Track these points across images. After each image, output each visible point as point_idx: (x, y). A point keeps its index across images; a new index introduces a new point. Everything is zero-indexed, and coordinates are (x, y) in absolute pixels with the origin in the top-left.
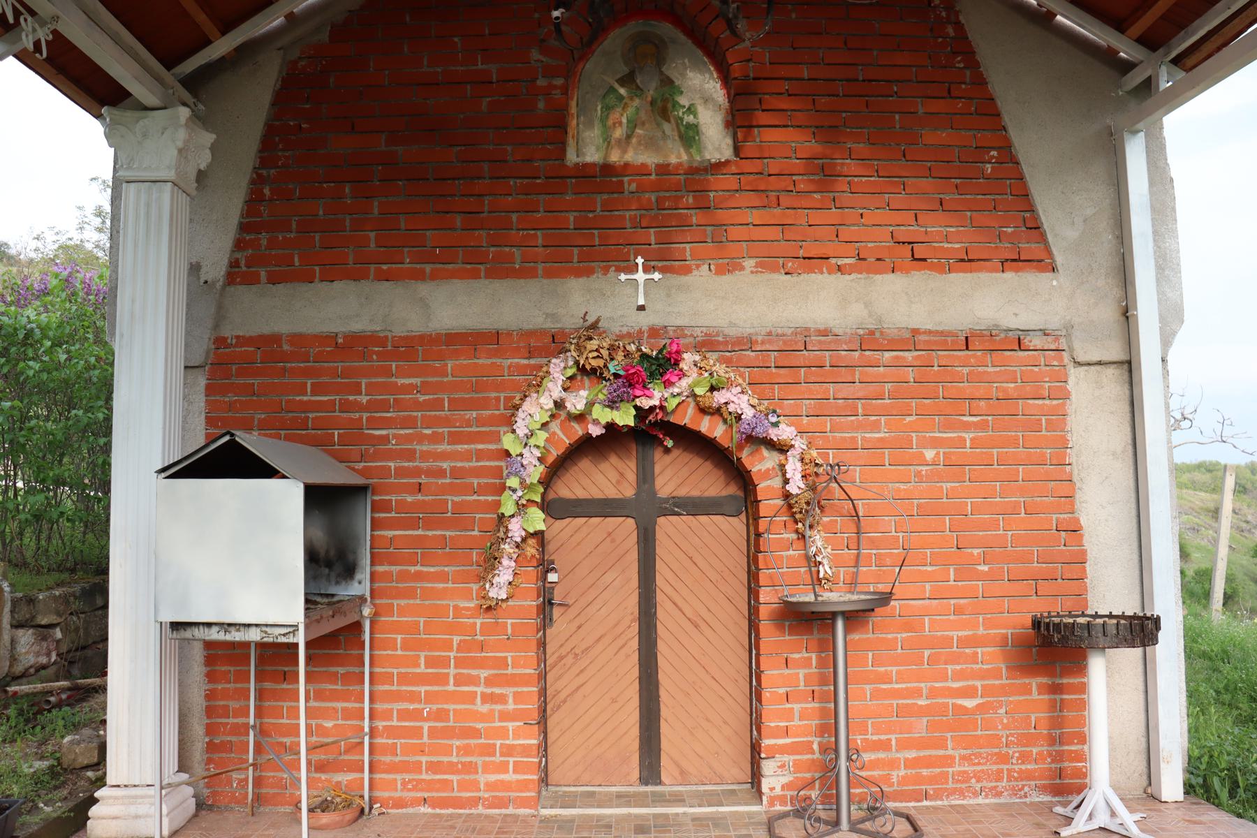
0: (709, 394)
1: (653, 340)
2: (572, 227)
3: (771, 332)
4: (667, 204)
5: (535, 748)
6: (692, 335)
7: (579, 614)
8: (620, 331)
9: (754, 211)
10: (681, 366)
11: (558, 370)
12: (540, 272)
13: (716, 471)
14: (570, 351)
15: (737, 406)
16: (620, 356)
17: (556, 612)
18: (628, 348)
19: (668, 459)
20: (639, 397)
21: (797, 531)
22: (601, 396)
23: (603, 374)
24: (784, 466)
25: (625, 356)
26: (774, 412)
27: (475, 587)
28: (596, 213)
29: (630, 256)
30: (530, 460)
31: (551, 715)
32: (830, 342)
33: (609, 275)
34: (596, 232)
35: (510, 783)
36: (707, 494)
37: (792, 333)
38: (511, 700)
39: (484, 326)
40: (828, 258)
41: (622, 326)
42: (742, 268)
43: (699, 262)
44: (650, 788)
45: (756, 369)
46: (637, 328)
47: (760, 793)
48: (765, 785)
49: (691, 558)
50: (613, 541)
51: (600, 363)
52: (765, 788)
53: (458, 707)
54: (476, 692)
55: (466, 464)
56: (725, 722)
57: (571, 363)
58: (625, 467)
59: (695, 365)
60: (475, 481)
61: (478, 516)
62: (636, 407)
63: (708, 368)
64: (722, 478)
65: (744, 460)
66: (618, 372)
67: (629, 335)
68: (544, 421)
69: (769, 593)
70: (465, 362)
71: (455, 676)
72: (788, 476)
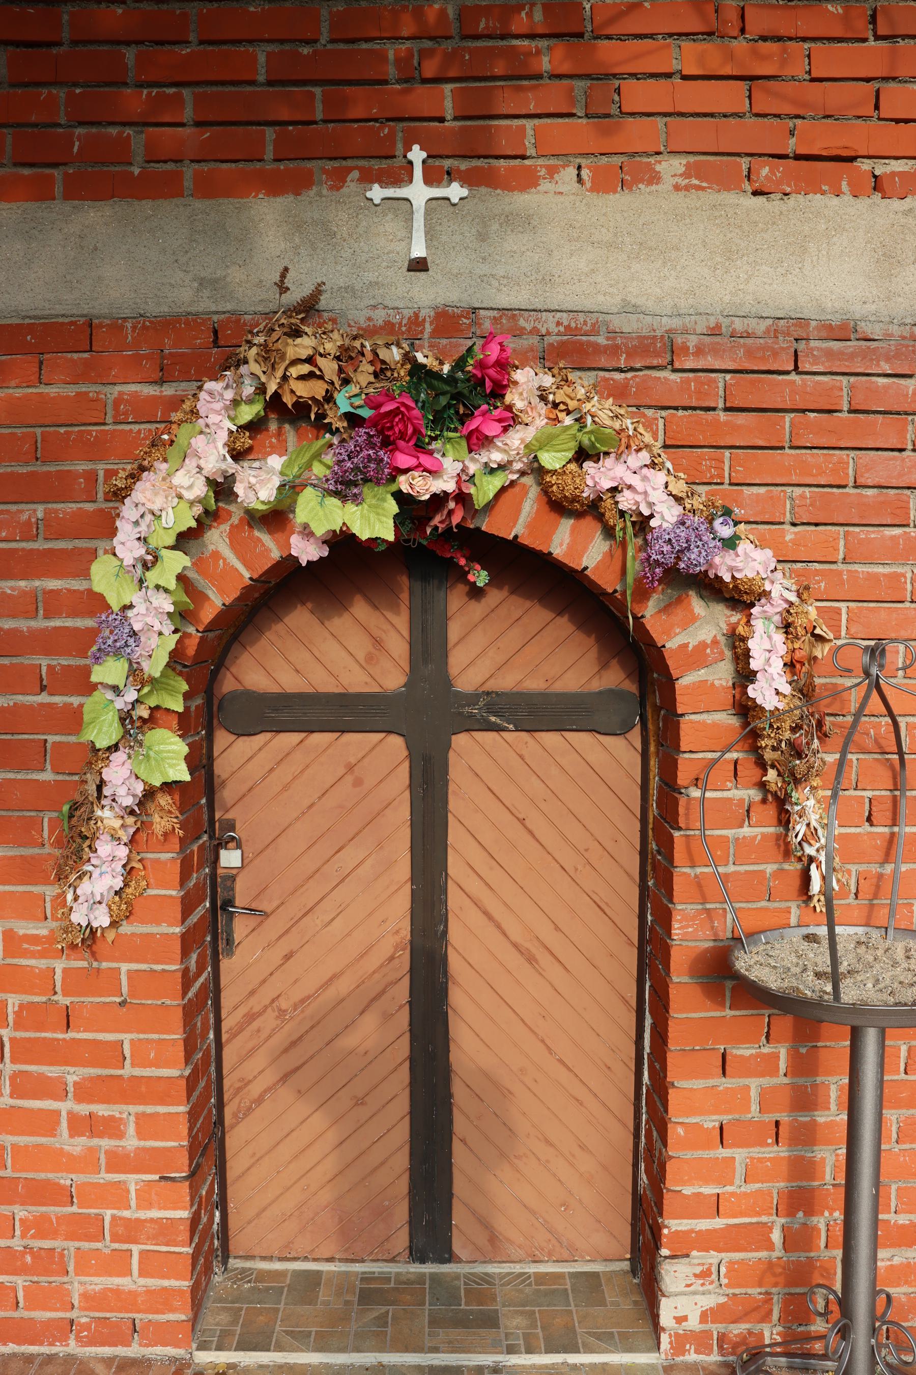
0: (573, 467)
1: (444, 341)
2: (261, 78)
3: (718, 326)
4: (482, 25)
5: (184, 1229)
6: (535, 331)
7: (287, 932)
8: (369, 319)
9: (686, 44)
10: (508, 399)
11: (218, 406)
12: (188, 183)
13: (579, 636)
14: (246, 362)
15: (639, 498)
16: (364, 374)
17: (241, 927)
18: (383, 354)
19: (477, 609)
20: (406, 471)
21: (762, 786)
22: (319, 470)
23: (324, 416)
24: (744, 639)
25: (376, 375)
26: (727, 512)
27: (50, 891)
28: (318, 46)
29: (394, 144)
30: (149, 620)
31: (233, 1127)
32: (852, 356)
33: (345, 190)
34: (318, 91)
35: (133, 1294)
36: (559, 687)
37: (768, 330)
38: (131, 1130)
39: (59, 309)
40: (852, 159)
41: (374, 307)
42: (655, 178)
43: (553, 162)
44: (429, 1268)
45: (680, 413)
46: (408, 313)
47: (657, 1328)
48: (667, 1315)
49: (522, 821)
50: (358, 782)
51: (317, 389)
52: (666, 1318)
53: (23, 1140)
54: (58, 1113)
55: (23, 624)
56: (582, 1147)
57: (248, 390)
58: (386, 626)
59: (543, 398)
60: (44, 662)
61: (51, 739)
62: (399, 496)
63: (572, 404)
64: (593, 654)
65: (650, 623)
66: (360, 412)
67: (389, 327)
68: (183, 528)
69: (694, 918)
70: (18, 393)
71: (13, 1078)
72: (754, 665)
